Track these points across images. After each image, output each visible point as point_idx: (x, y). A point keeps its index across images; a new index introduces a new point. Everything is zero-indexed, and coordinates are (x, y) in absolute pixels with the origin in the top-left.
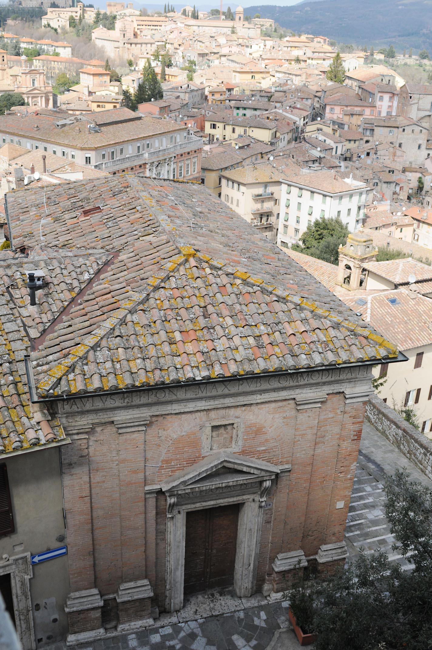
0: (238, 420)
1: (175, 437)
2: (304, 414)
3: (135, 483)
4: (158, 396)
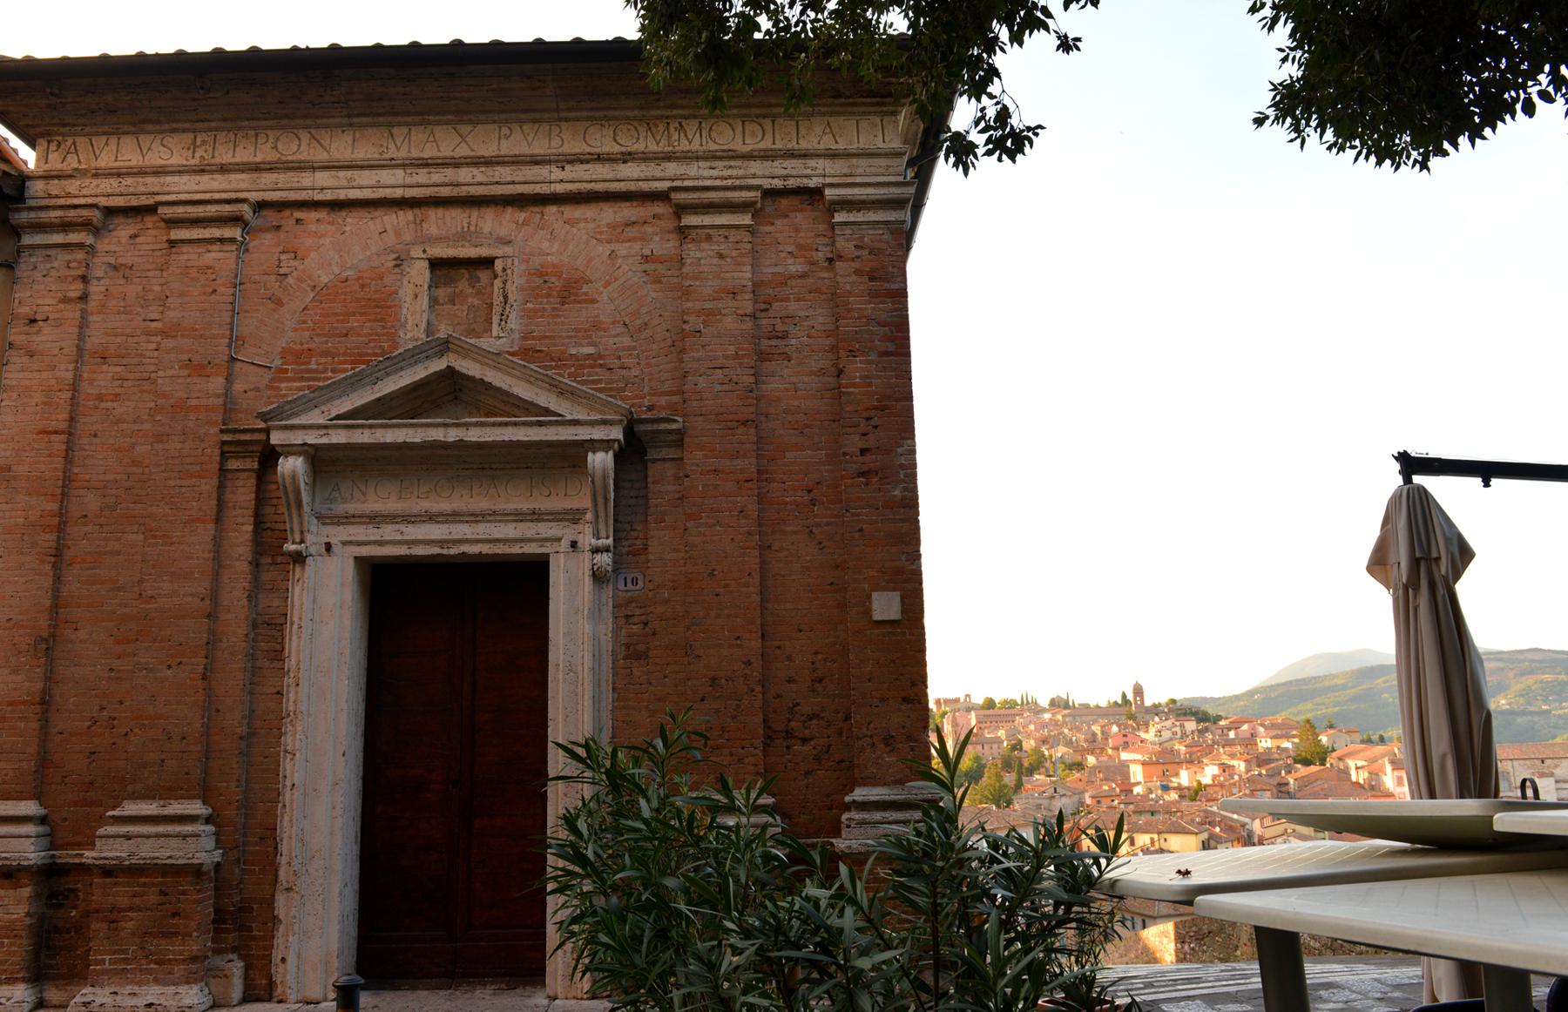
0: (508, 250)
1: (324, 279)
2: (705, 245)
3: (195, 408)
4: (280, 146)
